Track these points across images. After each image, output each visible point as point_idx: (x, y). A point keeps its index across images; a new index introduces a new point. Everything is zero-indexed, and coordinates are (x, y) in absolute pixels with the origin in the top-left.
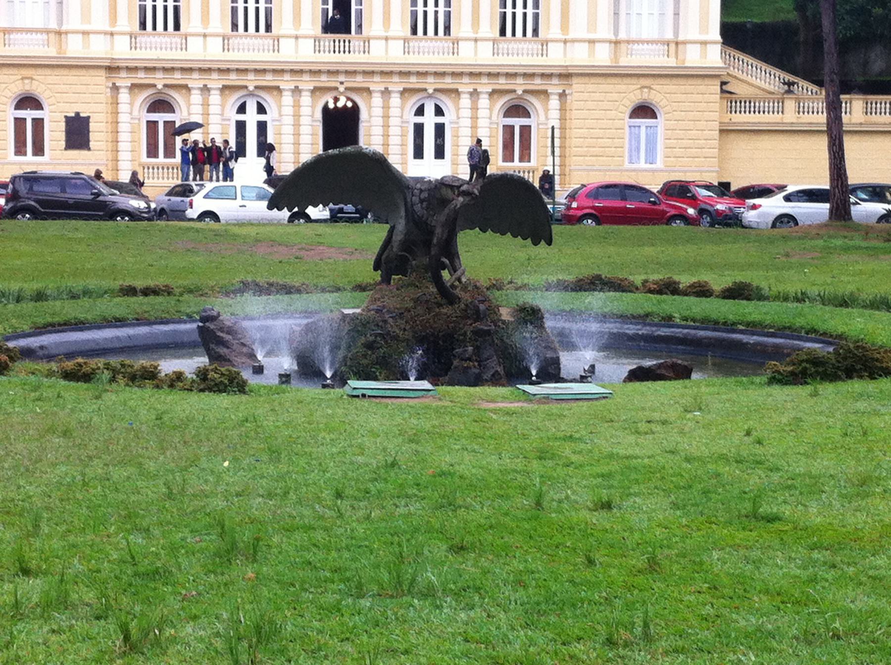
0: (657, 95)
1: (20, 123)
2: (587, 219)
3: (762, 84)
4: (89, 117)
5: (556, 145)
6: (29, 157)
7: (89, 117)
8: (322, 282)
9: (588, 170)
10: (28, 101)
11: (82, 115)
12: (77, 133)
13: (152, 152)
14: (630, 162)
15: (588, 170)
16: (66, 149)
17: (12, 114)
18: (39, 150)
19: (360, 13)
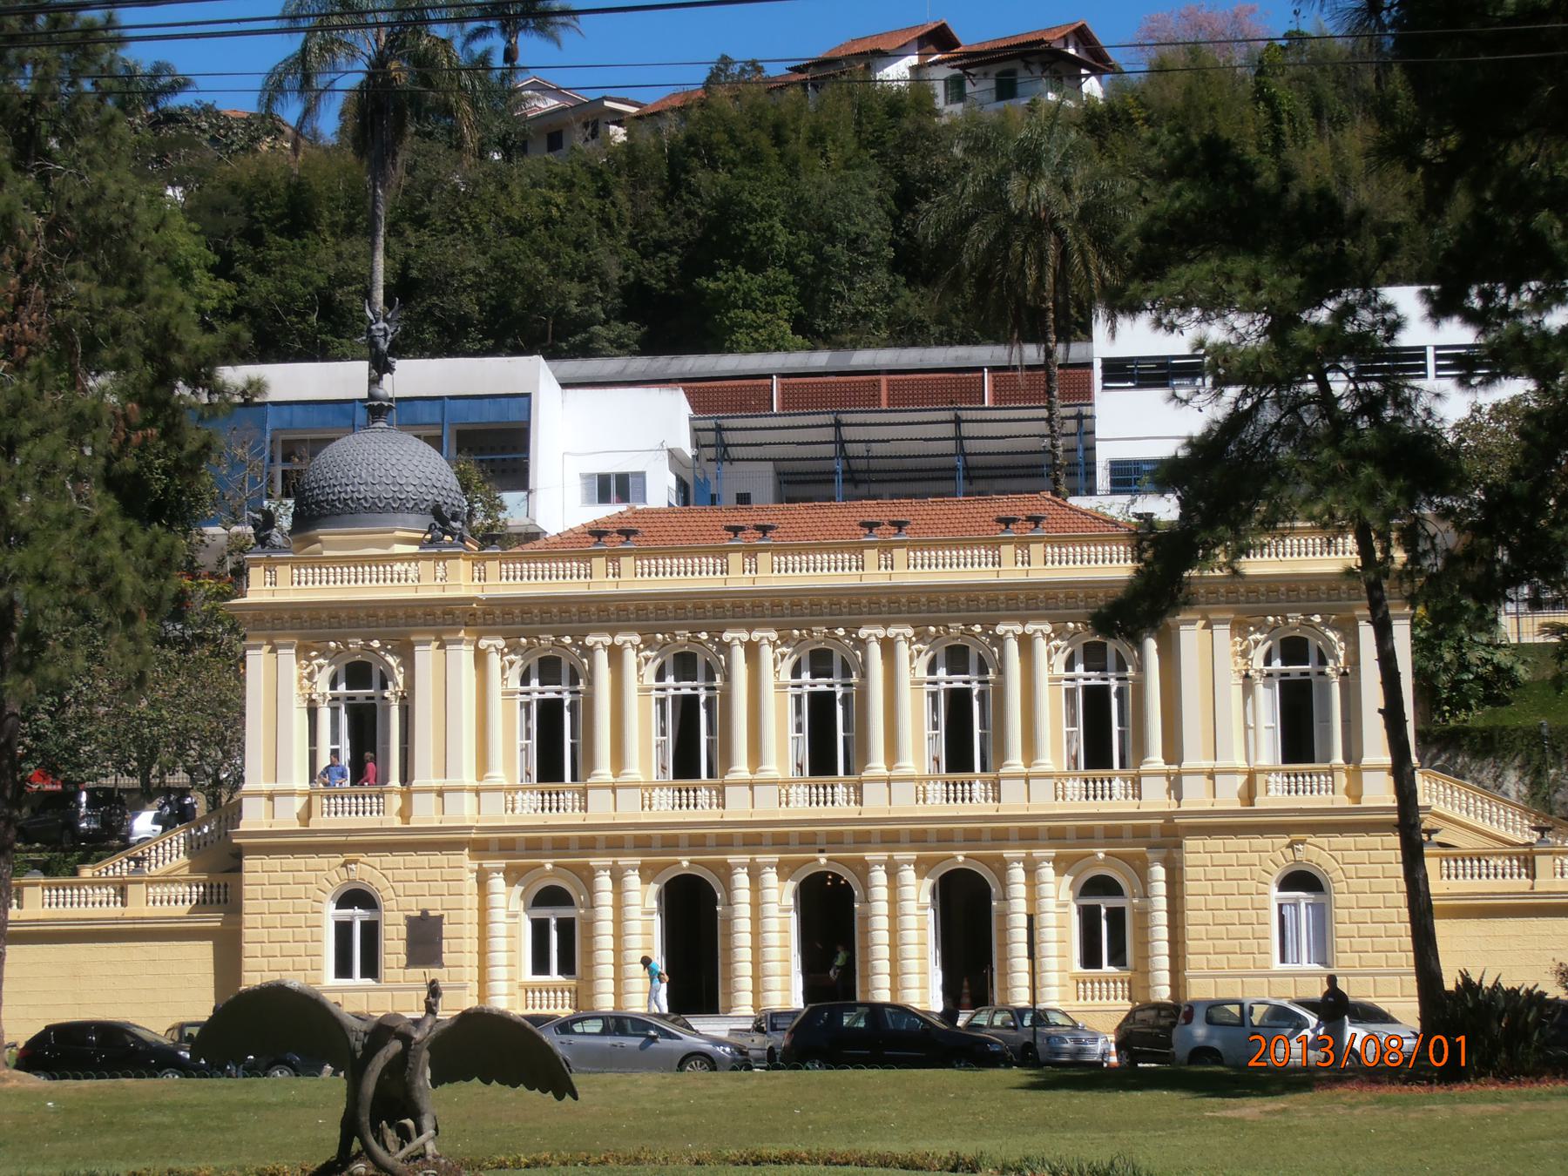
0: (1317, 853)
1: (343, 930)
2: (1307, 1069)
3: (1501, 831)
4: (441, 917)
5: (1025, 932)
6: (357, 980)
7: (441, 917)
8: (732, 1152)
9: (1214, 977)
10: (355, 897)
11: (432, 913)
12: (425, 940)
13: (540, 965)
14: (1283, 960)
15: (1214, 977)
16: (408, 966)
17: (331, 914)
18: (371, 970)
19: (1072, 722)
